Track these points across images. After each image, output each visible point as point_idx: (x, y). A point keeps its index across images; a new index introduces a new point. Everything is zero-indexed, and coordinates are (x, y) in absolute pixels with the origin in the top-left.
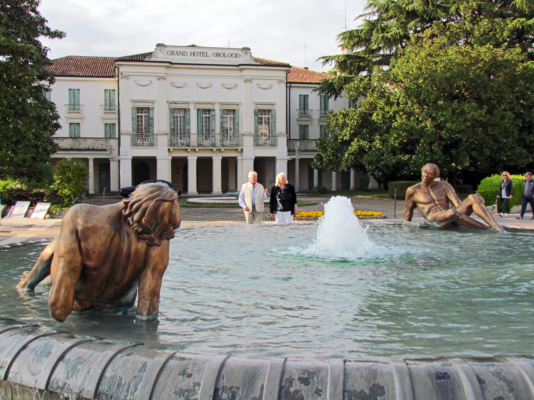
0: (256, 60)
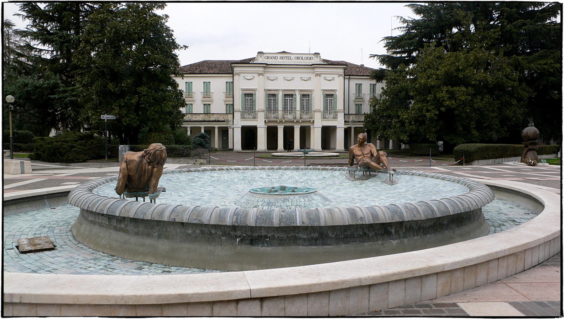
0: (324, 60)
